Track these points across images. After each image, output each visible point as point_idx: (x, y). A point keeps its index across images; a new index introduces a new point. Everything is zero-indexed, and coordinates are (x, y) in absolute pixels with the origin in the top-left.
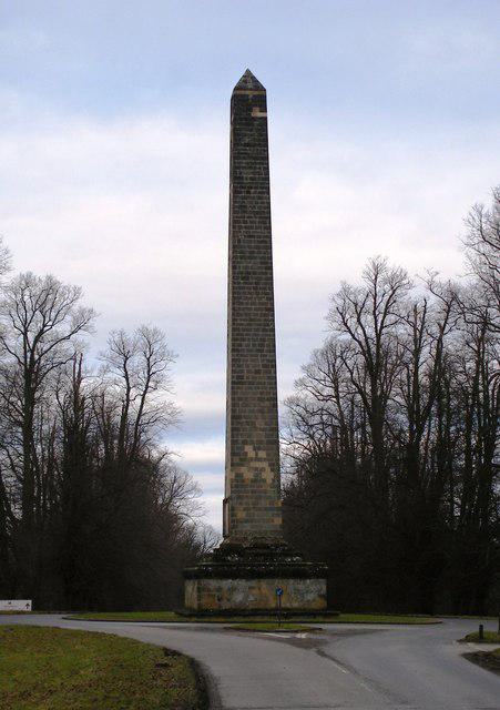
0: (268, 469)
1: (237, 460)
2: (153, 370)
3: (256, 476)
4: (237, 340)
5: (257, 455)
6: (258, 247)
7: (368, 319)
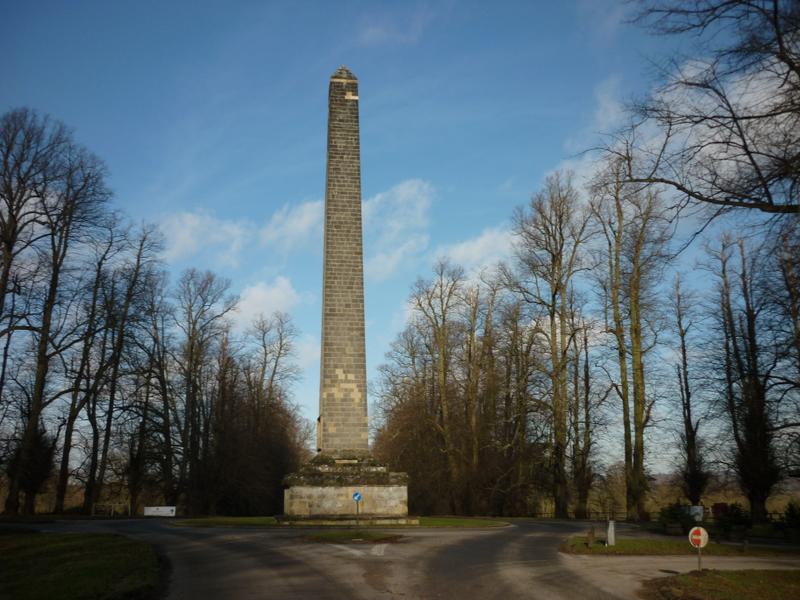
0: (356, 390)
1: (328, 381)
2: (284, 342)
3: (345, 395)
4: (330, 278)
5: (346, 377)
6: (348, 202)
7: (436, 302)
